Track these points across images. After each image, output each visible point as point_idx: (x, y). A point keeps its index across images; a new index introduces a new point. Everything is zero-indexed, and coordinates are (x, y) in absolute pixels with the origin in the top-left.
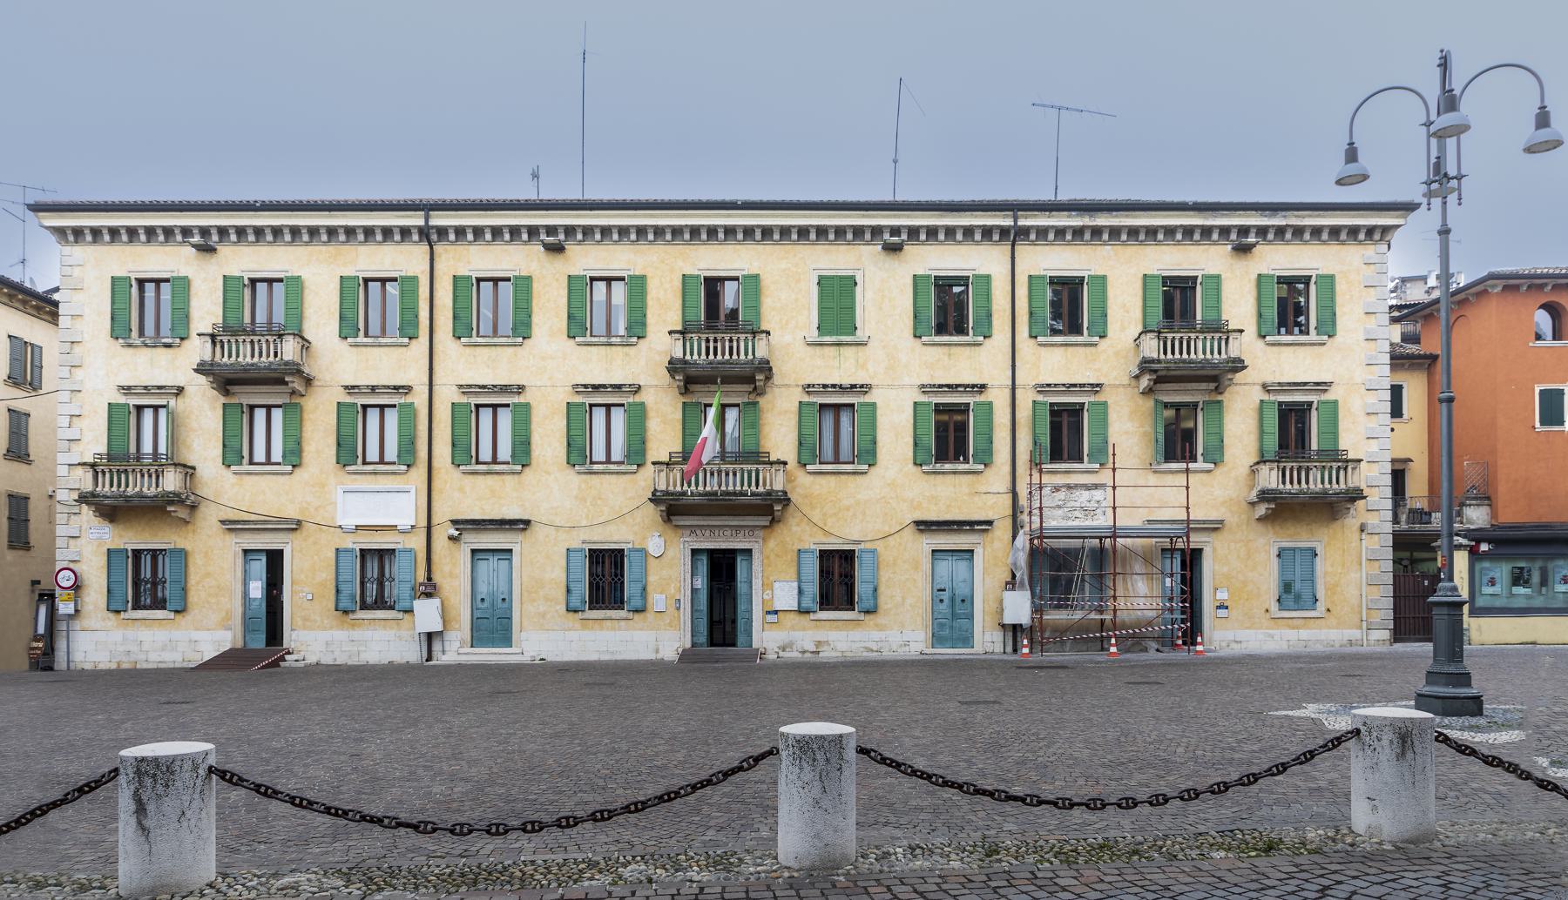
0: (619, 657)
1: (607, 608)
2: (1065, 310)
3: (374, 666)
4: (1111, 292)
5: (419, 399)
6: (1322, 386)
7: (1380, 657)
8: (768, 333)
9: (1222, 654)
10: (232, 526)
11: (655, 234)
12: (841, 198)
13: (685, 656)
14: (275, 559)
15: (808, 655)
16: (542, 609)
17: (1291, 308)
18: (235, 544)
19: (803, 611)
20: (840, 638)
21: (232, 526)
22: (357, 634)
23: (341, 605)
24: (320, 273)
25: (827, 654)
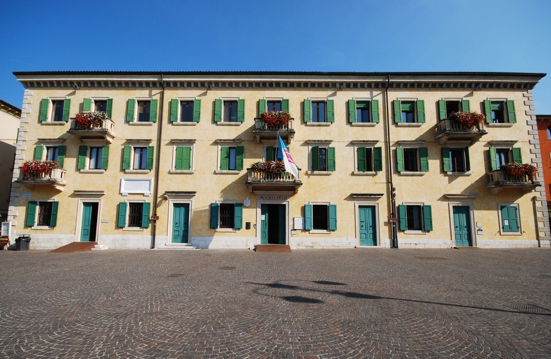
0: (231, 248)
1: (227, 227)
2: (6, 107)
3: (329, 251)
4: (246, 104)
5: (154, 144)
6: (329, 142)
7: (148, 251)
8: (293, 119)
9: (102, 249)
10: (77, 194)
11: (249, 85)
12: (239, 70)
13: (256, 248)
14: (95, 206)
15: (309, 248)
16: (200, 227)
17: (502, 114)
18: (80, 201)
19: (305, 230)
20: (319, 240)
21: (77, 194)
22: (126, 236)
23: (28, 224)
24: (295, 99)
25: (317, 247)
